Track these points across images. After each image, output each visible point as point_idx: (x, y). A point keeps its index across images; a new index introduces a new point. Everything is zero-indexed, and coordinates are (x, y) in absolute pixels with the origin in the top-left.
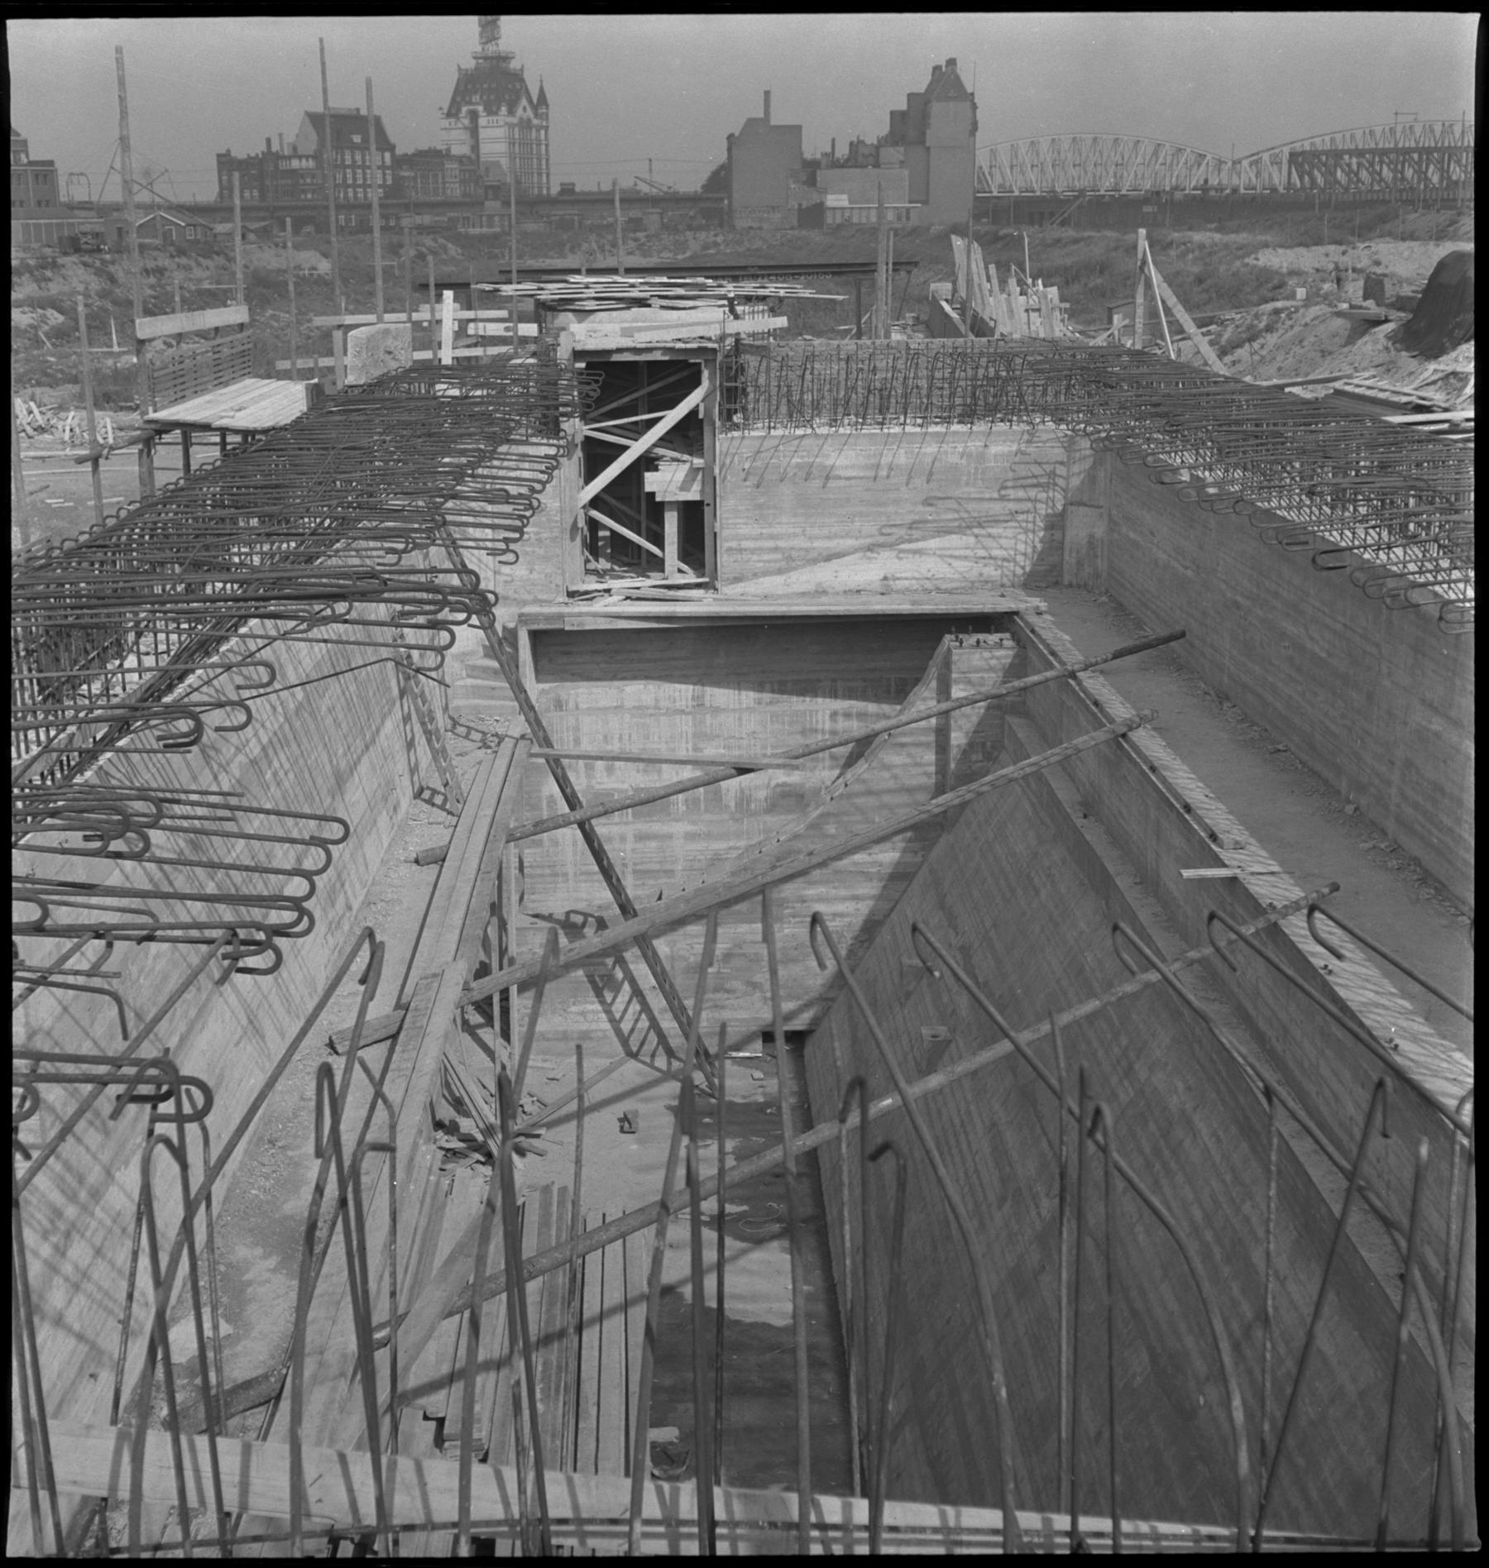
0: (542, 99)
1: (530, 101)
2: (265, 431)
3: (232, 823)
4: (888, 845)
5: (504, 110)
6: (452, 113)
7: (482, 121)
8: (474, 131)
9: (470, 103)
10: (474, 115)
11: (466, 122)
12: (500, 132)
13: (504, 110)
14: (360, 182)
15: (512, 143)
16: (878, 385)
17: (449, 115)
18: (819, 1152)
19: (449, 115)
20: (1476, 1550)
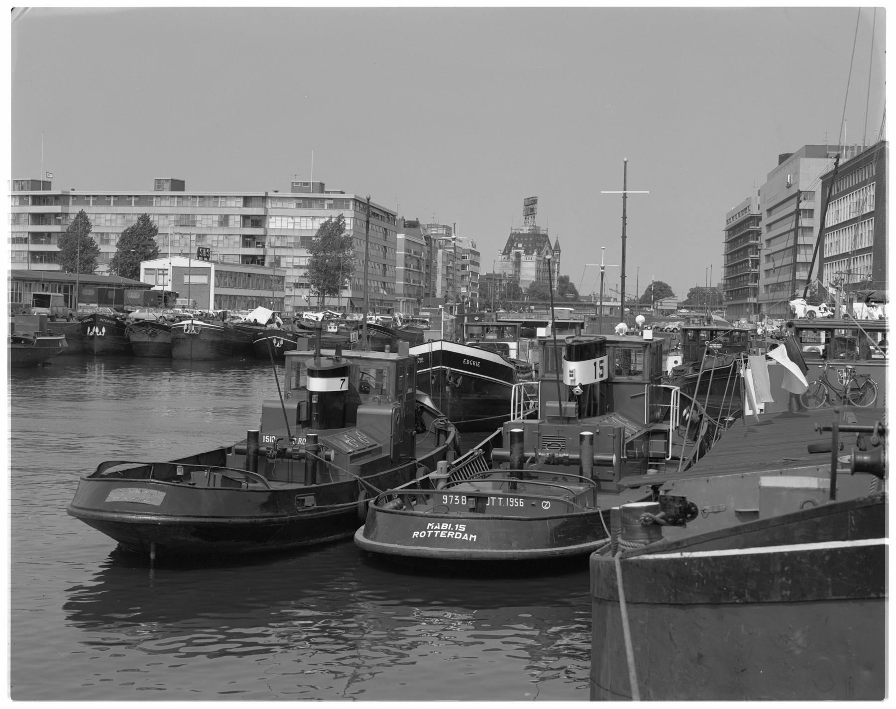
0: (557, 248)
1: (550, 247)
2: (12, 311)
3: (357, 659)
4: (617, 381)
5: (535, 253)
6: (507, 252)
7: (523, 258)
8: (517, 263)
9: (517, 248)
10: (518, 255)
11: (513, 258)
12: (533, 265)
13: (535, 253)
14: (862, 273)
15: (538, 270)
16: (634, 313)
17: (504, 254)
18: (876, 479)
19: (504, 254)
20: (88, 334)
